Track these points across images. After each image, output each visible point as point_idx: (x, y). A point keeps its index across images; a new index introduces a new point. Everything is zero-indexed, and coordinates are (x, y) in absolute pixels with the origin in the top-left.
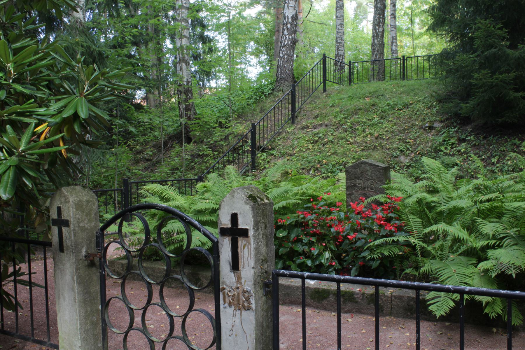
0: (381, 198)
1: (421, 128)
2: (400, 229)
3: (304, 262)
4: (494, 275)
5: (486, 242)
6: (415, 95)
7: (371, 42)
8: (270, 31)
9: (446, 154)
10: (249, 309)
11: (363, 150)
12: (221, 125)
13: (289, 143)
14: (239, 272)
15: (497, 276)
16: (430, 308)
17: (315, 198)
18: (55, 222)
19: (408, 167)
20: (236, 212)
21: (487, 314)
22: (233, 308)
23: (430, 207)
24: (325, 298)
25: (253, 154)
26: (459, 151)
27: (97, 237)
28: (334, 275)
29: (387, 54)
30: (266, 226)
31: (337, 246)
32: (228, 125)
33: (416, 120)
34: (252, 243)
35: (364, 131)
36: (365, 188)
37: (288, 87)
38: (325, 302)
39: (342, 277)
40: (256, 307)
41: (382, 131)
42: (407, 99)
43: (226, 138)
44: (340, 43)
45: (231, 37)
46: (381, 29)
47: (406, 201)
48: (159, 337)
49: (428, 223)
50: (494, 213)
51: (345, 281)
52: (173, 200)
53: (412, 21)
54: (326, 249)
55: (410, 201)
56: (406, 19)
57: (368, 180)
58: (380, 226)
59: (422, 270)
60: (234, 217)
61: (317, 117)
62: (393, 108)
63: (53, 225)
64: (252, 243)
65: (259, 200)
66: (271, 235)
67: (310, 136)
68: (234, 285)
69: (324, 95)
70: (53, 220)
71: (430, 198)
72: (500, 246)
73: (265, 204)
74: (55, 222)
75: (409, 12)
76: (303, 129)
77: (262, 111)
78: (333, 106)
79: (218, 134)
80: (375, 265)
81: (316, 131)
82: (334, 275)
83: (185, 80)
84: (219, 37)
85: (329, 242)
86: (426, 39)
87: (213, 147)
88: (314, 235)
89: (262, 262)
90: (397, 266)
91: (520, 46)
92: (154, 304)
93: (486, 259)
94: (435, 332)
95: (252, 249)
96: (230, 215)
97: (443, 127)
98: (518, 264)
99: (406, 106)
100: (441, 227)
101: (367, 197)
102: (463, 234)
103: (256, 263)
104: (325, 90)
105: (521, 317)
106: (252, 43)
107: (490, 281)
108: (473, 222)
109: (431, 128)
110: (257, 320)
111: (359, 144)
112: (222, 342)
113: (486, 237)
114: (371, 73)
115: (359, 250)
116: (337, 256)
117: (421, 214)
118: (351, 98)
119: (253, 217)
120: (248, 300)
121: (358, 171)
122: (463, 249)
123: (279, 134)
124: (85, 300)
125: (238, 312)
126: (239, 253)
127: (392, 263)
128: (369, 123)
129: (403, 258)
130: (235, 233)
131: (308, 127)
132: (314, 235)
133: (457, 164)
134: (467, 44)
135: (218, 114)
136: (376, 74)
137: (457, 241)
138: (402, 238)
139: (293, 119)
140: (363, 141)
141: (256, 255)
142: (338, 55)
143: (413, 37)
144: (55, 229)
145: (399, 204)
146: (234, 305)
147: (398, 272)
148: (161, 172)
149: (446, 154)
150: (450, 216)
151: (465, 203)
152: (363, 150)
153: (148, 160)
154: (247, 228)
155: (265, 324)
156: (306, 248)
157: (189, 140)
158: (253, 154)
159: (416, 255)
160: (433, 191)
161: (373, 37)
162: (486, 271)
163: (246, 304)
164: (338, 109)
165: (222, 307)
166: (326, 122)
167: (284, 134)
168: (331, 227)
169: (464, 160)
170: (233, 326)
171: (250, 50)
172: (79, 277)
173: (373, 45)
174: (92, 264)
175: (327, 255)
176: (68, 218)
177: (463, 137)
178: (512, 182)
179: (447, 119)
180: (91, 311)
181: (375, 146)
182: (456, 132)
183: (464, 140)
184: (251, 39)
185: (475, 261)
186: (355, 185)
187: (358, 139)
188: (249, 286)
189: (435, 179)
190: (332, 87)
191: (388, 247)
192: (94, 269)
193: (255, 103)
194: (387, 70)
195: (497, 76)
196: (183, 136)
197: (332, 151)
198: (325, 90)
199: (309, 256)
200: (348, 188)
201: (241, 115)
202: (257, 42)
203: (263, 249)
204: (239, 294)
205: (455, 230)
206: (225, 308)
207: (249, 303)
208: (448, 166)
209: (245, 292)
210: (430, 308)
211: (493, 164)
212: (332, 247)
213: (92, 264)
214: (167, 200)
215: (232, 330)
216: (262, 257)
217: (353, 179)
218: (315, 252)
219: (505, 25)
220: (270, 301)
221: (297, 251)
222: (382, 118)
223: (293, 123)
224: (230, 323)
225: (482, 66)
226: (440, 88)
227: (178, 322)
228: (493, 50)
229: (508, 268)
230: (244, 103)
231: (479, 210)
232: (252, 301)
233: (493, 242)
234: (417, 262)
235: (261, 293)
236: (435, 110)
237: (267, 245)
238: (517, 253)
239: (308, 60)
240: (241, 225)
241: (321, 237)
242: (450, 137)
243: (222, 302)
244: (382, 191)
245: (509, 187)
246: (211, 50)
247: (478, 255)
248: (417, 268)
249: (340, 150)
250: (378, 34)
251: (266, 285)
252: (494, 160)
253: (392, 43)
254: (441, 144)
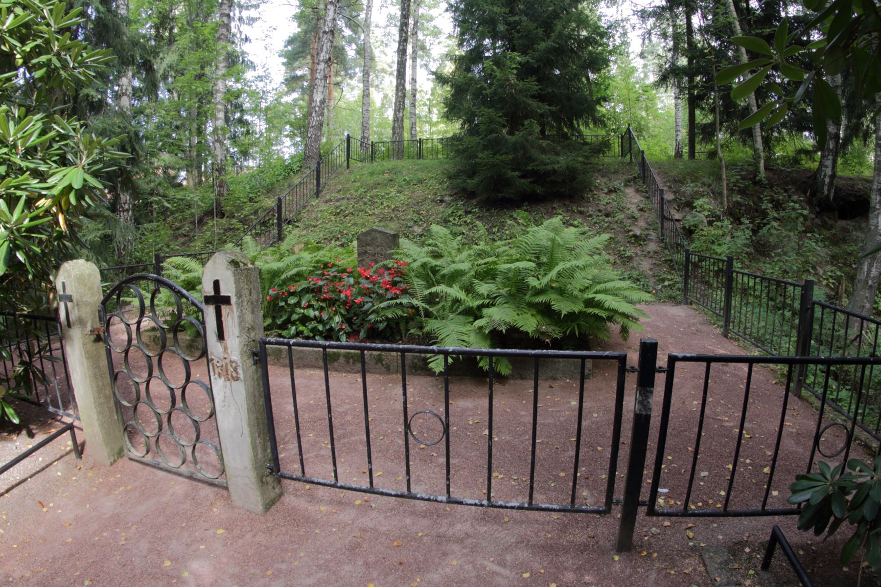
0: (390, 263)
1: (433, 201)
2: (405, 292)
3: (316, 327)
4: (487, 332)
5: (481, 302)
6: (429, 172)
7: (391, 126)
8: (304, 116)
9: (454, 224)
11: (380, 221)
12: (251, 200)
13: (314, 216)
15: (491, 332)
16: (431, 365)
17: (326, 266)
19: (421, 236)
21: (481, 368)
22: (223, 379)
23: (434, 270)
24: (335, 360)
25: (279, 225)
26: (465, 222)
28: (322, 342)
29: (406, 136)
30: (251, 292)
31: (347, 311)
32: (257, 199)
33: (428, 194)
34: (235, 311)
35: (382, 204)
37: (315, 163)
38: (336, 364)
39: (327, 343)
40: (245, 377)
41: (398, 204)
42: (421, 175)
43: (256, 213)
44: (365, 127)
45: (268, 121)
46: (401, 115)
47: (412, 265)
49: (430, 285)
50: (488, 274)
51: (330, 347)
52: (194, 271)
53: (430, 111)
54: (336, 312)
55: (415, 265)
56: (426, 109)
58: (387, 290)
59: (425, 330)
60: (216, 284)
61: (339, 191)
62: (408, 183)
64: (235, 311)
65: (241, 265)
66: (257, 301)
67: (332, 209)
68: (222, 356)
69: (348, 171)
71: (434, 262)
72: (493, 305)
73: (249, 269)
75: (428, 103)
76: (326, 202)
77: (289, 186)
78: (355, 181)
79: (247, 210)
80: (382, 326)
81: (338, 204)
82: (322, 342)
83: (219, 158)
84: (257, 121)
85: (339, 306)
86: (442, 127)
87: (243, 221)
88: (324, 300)
90: (402, 327)
91: (517, 133)
93: (481, 317)
94: (437, 386)
95: (236, 317)
97: (452, 200)
98: (508, 320)
99: (420, 181)
100: (441, 288)
101: (376, 262)
102: (461, 295)
103: (241, 331)
104: (348, 167)
105: (511, 367)
106: (288, 127)
107: (485, 337)
108: (471, 283)
109: (442, 201)
110: (247, 391)
111: (378, 216)
113: (481, 296)
114: (391, 152)
115: (366, 313)
116: (348, 320)
117: (426, 278)
118: (372, 174)
119: (235, 283)
120: (235, 370)
121: (369, 238)
122: (461, 308)
123: (304, 207)
124: (95, 375)
125: (228, 382)
127: (397, 324)
128: (387, 196)
129: (408, 320)
130: (218, 300)
131: (331, 201)
132: (324, 300)
133: (463, 234)
134: (473, 131)
135: (248, 190)
136: (395, 152)
137: (457, 301)
138: (405, 300)
139: (318, 194)
140: (381, 213)
141: (240, 324)
142: (363, 137)
143: (430, 123)
145: (405, 269)
147: (403, 332)
148: (195, 246)
149: (454, 224)
150: (452, 278)
151: (465, 266)
152: (380, 221)
153: (185, 236)
155: (257, 394)
156: (317, 313)
157: (222, 215)
158: (279, 225)
159: (420, 315)
160: (437, 255)
161: (394, 121)
162: (481, 328)
164: (359, 184)
165: (212, 378)
166: (348, 196)
167: (309, 208)
168: (340, 292)
169: (470, 229)
171: (286, 133)
172: (87, 352)
173: (394, 128)
174: (98, 339)
175: (337, 319)
177: (469, 209)
178: (507, 248)
179: (456, 194)
180: (103, 384)
181: (392, 218)
182: (464, 205)
183: (470, 212)
184: (286, 123)
185: (471, 319)
186: (366, 252)
187: (377, 211)
188: (235, 356)
189: (441, 245)
190: (355, 164)
191: (393, 309)
192: (101, 343)
193: (284, 179)
194: (406, 151)
195: (498, 156)
196: (217, 211)
197: (353, 222)
198: (348, 167)
199: (319, 320)
200: (359, 255)
201: (269, 190)
202: (292, 125)
203: (249, 317)
204: (226, 364)
205: (455, 291)
207: (237, 373)
208: (455, 235)
209: (231, 362)
210: (431, 365)
211: (494, 233)
212: (342, 311)
213: (98, 339)
214: (189, 271)
216: (247, 325)
218: (325, 317)
219: (505, 115)
220: (260, 370)
221: (309, 317)
222: (398, 192)
223: (318, 197)
224: (222, 394)
225: (485, 147)
226: (450, 167)
227: (178, 393)
228: (494, 135)
229: (499, 325)
230: (274, 180)
231: (476, 272)
232: (240, 371)
233: (487, 301)
234: (421, 322)
235: (250, 362)
236: (445, 186)
237: (253, 312)
238: (508, 310)
239: (333, 140)
240: (224, 293)
241: (331, 302)
242: (458, 209)
243: (212, 373)
244: (390, 257)
245: (504, 252)
246: (248, 133)
247: (474, 314)
248: (421, 328)
249: (360, 221)
250: (398, 120)
251: (254, 354)
252: (495, 230)
253: (412, 128)
254: (450, 216)
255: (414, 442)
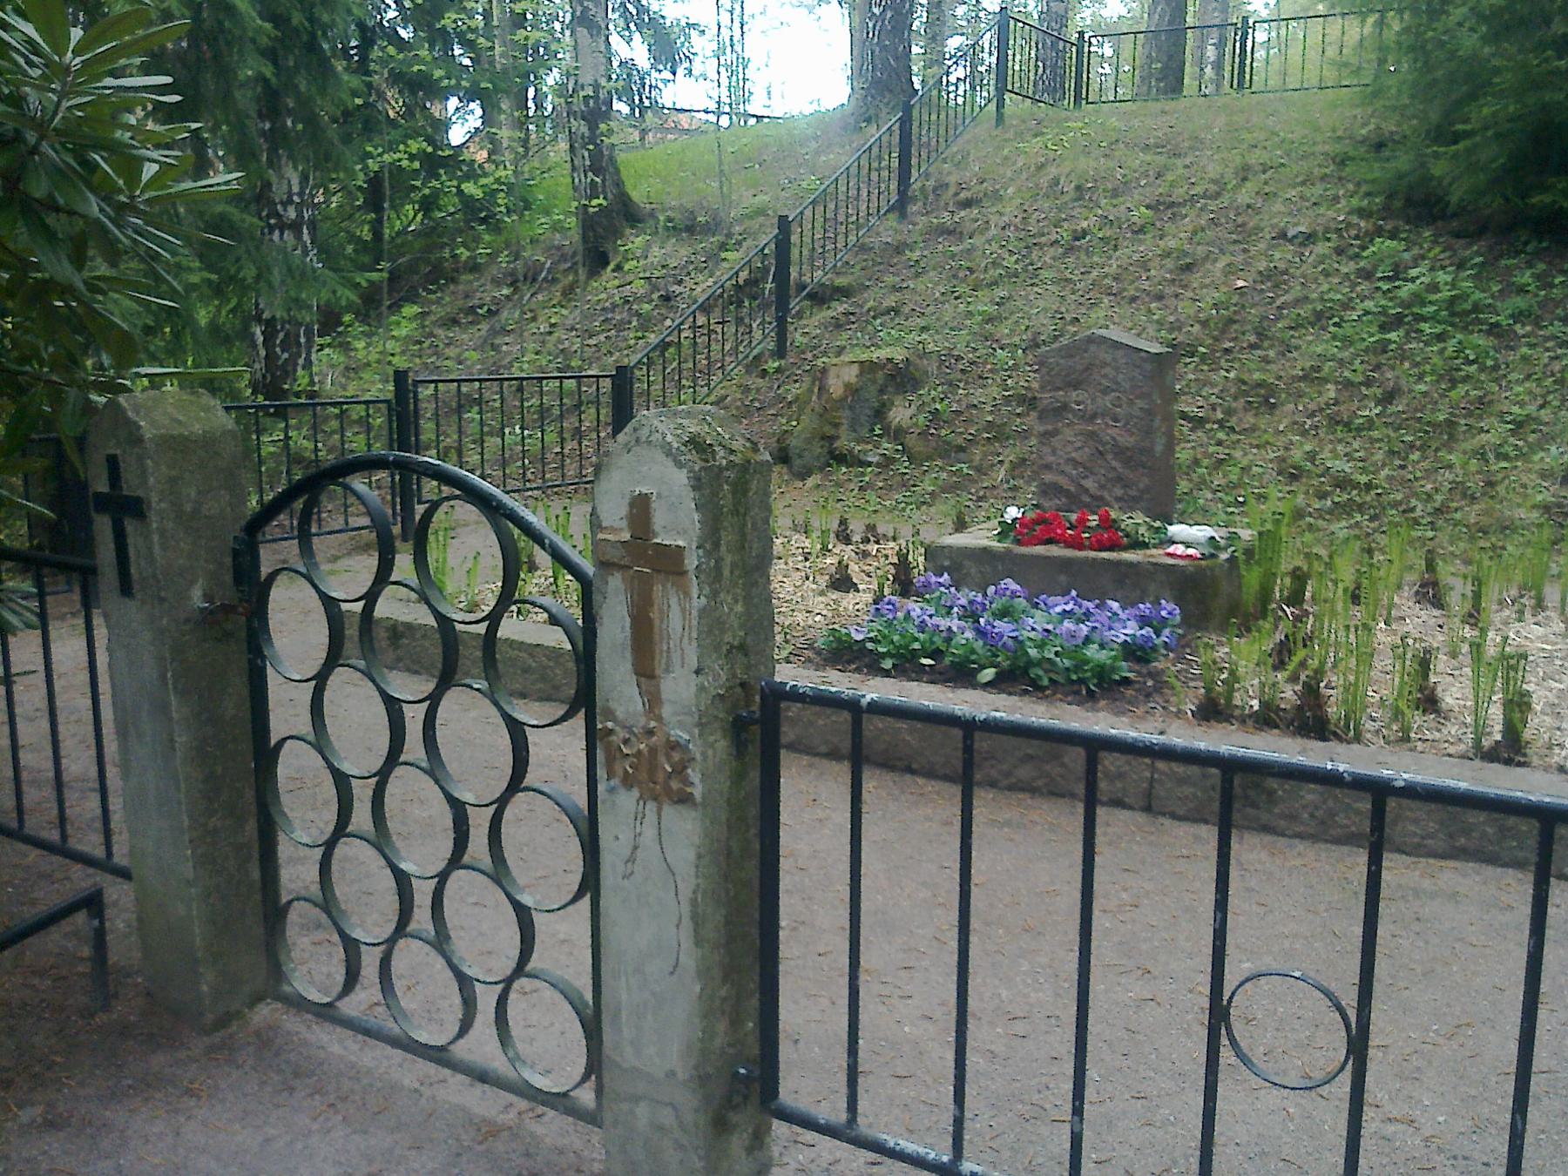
10: (684, 799)
14: (653, 682)
18: (103, 503)
20: (644, 491)
22: (636, 793)
27: (236, 554)
34: (695, 592)
36: (1094, 416)
48: (477, 789)
57: (1106, 391)
60: (640, 508)
63: (97, 511)
64: (695, 592)
70: (97, 495)
74: (103, 503)
89: (729, 652)
92: (406, 764)
96: (627, 500)
112: (602, 874)
120: (680, 770)
126: (657, 623)
144: (103, 525)
146: (640, 783)
154: (681, 543)
163: (675, 785)
170: (636, 848)
176: (140, 493)
206: (612, 790)
209: (674, 746)
215: (631, 859)
216: (728, 638)
217: (1059, 389)
224: (626, 837)
227: (423, 893)
232: (694, 775)
243: (601, 773)
255: (1233, 1060)
